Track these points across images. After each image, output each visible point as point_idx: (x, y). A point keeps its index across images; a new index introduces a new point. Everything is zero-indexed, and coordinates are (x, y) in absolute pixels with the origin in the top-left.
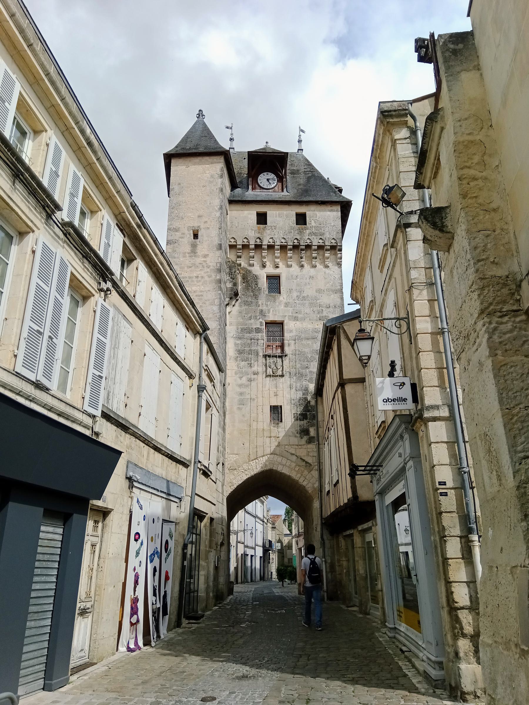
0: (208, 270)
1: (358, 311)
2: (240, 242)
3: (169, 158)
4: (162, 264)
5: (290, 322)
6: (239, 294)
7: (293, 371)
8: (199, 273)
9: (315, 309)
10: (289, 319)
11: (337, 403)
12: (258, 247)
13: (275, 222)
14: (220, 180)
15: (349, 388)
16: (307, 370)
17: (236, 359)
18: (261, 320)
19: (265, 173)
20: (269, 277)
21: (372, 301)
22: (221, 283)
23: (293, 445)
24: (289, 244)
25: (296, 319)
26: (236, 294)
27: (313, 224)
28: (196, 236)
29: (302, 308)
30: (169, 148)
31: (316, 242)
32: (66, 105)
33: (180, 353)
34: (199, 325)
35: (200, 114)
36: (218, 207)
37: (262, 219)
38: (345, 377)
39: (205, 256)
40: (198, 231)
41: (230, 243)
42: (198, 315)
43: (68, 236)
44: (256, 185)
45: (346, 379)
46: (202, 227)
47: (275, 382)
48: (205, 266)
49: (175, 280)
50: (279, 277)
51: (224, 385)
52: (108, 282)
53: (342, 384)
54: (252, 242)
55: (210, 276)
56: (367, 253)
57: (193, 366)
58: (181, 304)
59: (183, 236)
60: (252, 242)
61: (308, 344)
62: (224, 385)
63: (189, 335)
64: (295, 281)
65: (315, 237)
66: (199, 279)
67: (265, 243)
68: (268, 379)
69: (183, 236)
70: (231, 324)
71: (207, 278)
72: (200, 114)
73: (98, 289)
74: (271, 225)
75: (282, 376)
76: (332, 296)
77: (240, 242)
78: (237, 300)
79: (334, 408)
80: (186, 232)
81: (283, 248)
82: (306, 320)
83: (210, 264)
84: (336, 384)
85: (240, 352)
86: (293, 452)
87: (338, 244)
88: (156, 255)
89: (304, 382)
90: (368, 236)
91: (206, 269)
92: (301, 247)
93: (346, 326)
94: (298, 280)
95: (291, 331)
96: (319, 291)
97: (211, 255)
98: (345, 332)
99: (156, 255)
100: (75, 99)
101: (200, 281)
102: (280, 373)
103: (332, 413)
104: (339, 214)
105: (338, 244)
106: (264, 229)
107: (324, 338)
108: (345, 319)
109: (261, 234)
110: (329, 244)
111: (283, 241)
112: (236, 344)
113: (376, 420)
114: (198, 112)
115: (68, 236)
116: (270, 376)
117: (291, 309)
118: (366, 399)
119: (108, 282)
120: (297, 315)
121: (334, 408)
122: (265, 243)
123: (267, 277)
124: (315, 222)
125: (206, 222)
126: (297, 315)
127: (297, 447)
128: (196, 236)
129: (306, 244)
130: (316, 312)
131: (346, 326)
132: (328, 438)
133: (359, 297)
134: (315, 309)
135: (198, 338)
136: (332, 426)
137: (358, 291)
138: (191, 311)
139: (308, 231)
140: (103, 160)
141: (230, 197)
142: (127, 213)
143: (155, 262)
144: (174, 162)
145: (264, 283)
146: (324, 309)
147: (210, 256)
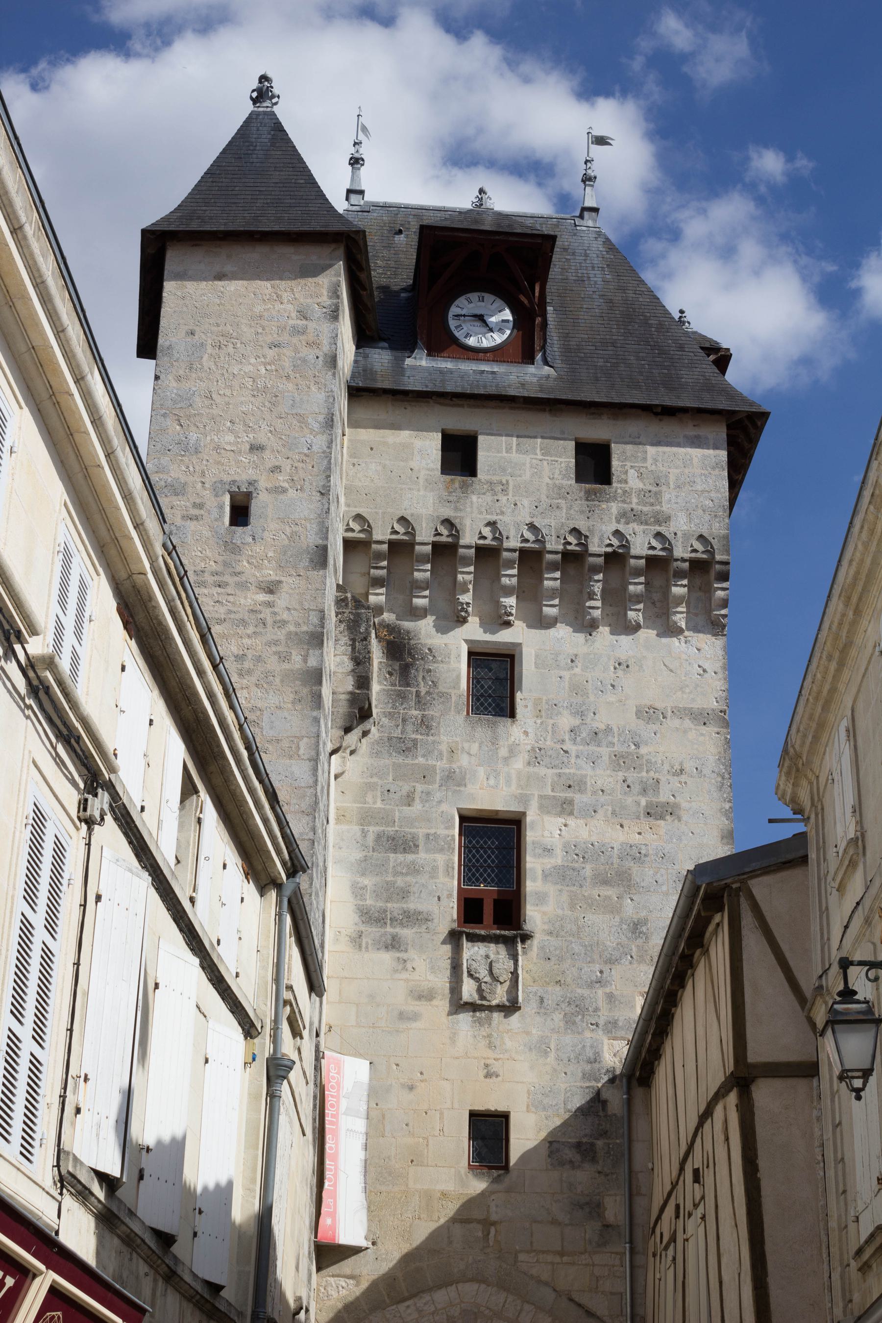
0: (281, 635)
1: (801, 837)
2: (382, 533)
3: (158, 250)
4: (211, 696)
5: (546, 818)
6: (375, 711)
7: (554, 993)
8: (247, 641)
9: (632, 776)
10: (544, 809)
11: (720, 1137)
12: (445, 552)
13: (504, 470)
14: (326, 328)
15: (765, 1093)
16: (600, 992)
17: (357, 940)
18: (444, 807)
19: (474, 296)
20: (479, 658)
21: (854, 841)
22: (320, 683)
23: (543, 1252)
24: (549, 547)
25: (565, 808)
26: (364, 714)
27: (634, 482)
28: (240, 513)
29: (590, 772)
30: (162, 201)
31: (641, 544)
32: (60, 331)
33: (228, 960)
34: (284, 863)
35: (263, 93)
36: (321, 418)
37: (460, 456)
38: (756, 1054)
39: (271, 588)
40: (248, 495)
41: (350, 535)
42: (282, 829)
43: (42, 694)
44: (443, 342)
45: (755, 1066)
46: (263, 484)
47: (485, 1030)
48: (269, 621)
49: (237, 735)
50: (512, 657)
51: (317, 1035)
52: (100, 791)
53: (742, 1079)
54: (425, 535)
55: (284, 658)
56: (841, 687)
57: (252, 990)
58: (240, 803)
59: (196, 512)
60: (425, 535)
61: (608, 898)
62: (317, 1035)
63: (250, 889)
64: (566, 674)
65: (639, 528)
66: (247, 665)
67: (469, 538)
68: (465, 1018)
69: (196, 512)
70: (341, 817)
71: (273, 664)
72: (263, 93)
73: (79, 818)
74: (488, 477)
75: (511, 1007)
76: (692, 735)
77: (382, 533)
78: (365, 734)
79: (708, 1146)
80: (211, 502)
81: (531, 559)
82: (601, 812)
83: (285, 616)
84: (716, 1077)
85: (368, 916)
86: (545, 1277)
87: (718, 557)
88: (201, 673)
89: (588, 1034)
90: (849, 644)
91: (271, 633)
92: (591, 560)
93: (760, 887)
94: (577, 670)
95: (548, 851)
96: (649, 714)
97: (290, 583)
98: (751, 897)
99: (201, 673)
100: (82, 317)
101: (249, 672)
102: (500, 995)
103: (696, 1160)
104: (723, 455)
105: (718, 557)
106: (464, 487)
107: (683, 914)
108: (755, 865)
109: (456, 509)
110: (687, 555)
111: (528, 535)
112: (358, 891)
113: (852, 1213)
114: (255, 84)
115: (42, 694)
116: (473, 1007)
117: (550, 772)
118: (817, 1133)
119: (100, 791)
120: (569, 794)
121: (708, 1146)
122: (469, 538)
123: (470, 654)
124: (641, 476)
125: (276, 469)
126: (569, 794)
127: (557, 1259)
128: (240, 513)
129: (609, 550)
130: (636, 788)
131: (760, 887)
132: (673, 1239)
133: (804, 797)
134: (632, 776)
135: (273, 894)
136: (696, 1206)
137: (804, 783)
138: (266, 821)
139: (614, 508)
140: (119, 453)
141: (353, 376)
142: (150, 576)
143: (196, 694)
144: (173, 260)
145: (458, 677)
146: (663, 779)
147: (285, 588)
